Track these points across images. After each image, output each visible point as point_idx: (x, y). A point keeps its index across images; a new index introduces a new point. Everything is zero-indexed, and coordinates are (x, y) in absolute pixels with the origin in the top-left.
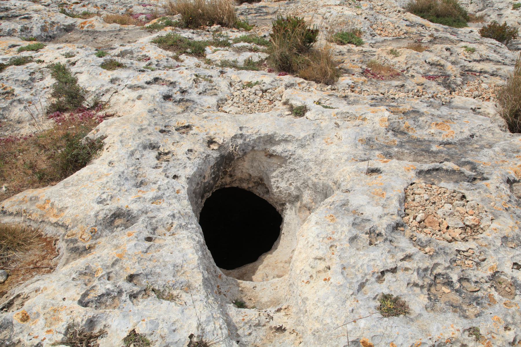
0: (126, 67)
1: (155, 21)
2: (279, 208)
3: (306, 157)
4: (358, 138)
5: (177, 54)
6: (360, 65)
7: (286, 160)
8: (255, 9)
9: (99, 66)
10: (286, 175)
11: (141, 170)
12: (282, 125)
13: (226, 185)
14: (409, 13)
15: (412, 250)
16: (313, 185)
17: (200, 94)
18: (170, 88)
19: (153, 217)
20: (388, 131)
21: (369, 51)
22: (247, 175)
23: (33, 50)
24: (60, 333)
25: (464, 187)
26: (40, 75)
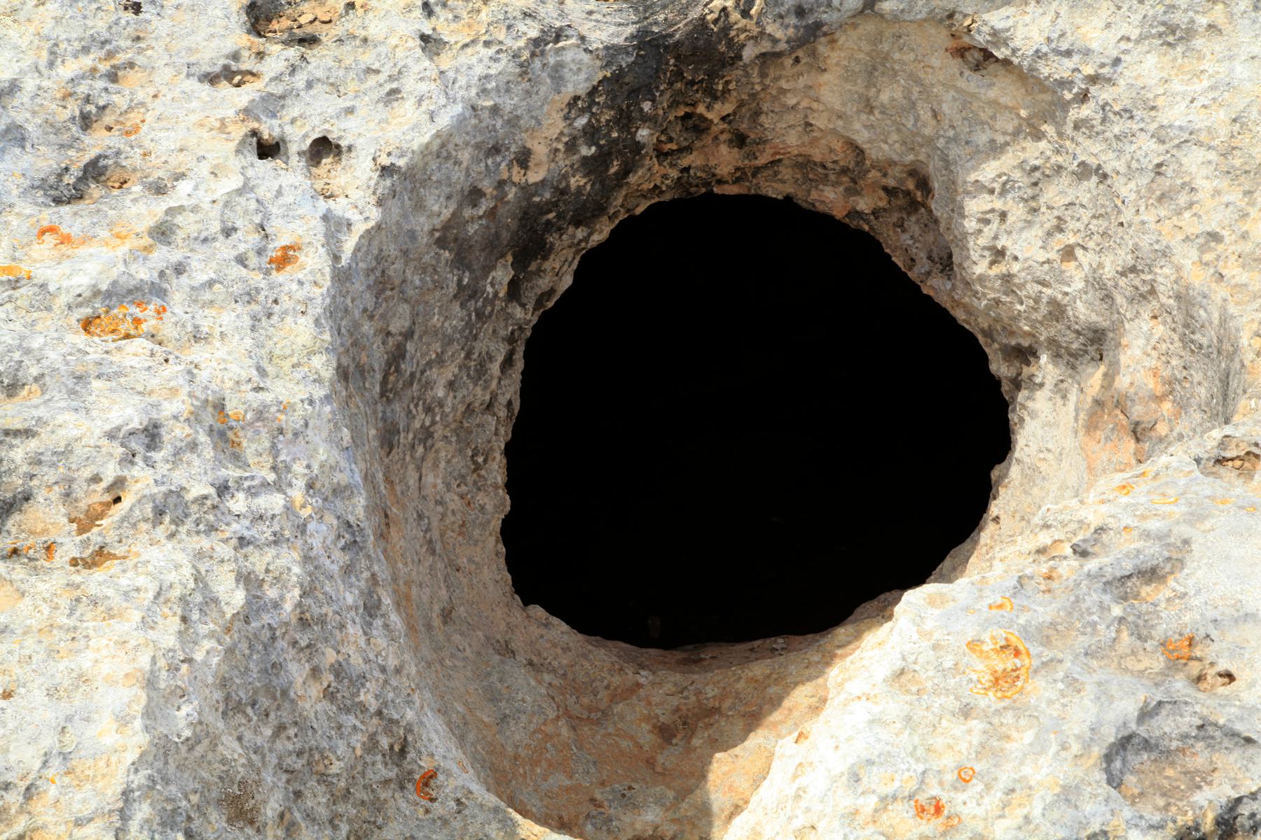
2: (1000, 367)
3: (1175, 114)
7: (1065, 106)
10: (1055, 194)
11: (132, 76)
16: (1178, 297)
19: (16, 433)
22: (837, 146)
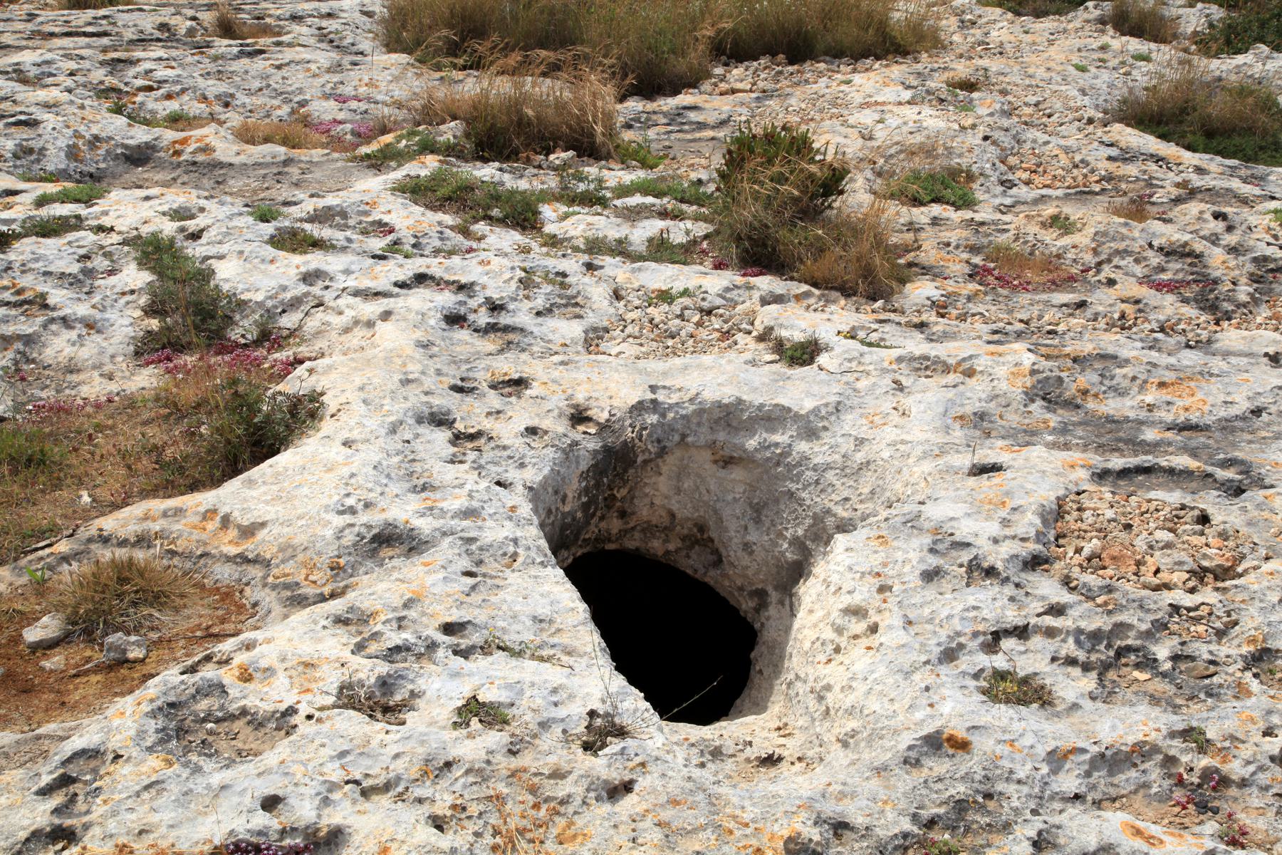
0: (333, 247)
1: (388, 138)
2: (746, 605)
4: (952, 413)
5: (465, 221)
6: (965, 256)
8: (665, 114)
9: (267, 243)
12: (757, 384)
13: (610, 540)
14: (1118, 127)
15: (1065, 597)
17: (539, 314)
18: (461, 297)
20: (1033, 401)
21: (994, 223)
22: (664, 514)
23: (78, 201)
24: (327, 693)
25: (1209, 501)
26: (107, 263)
